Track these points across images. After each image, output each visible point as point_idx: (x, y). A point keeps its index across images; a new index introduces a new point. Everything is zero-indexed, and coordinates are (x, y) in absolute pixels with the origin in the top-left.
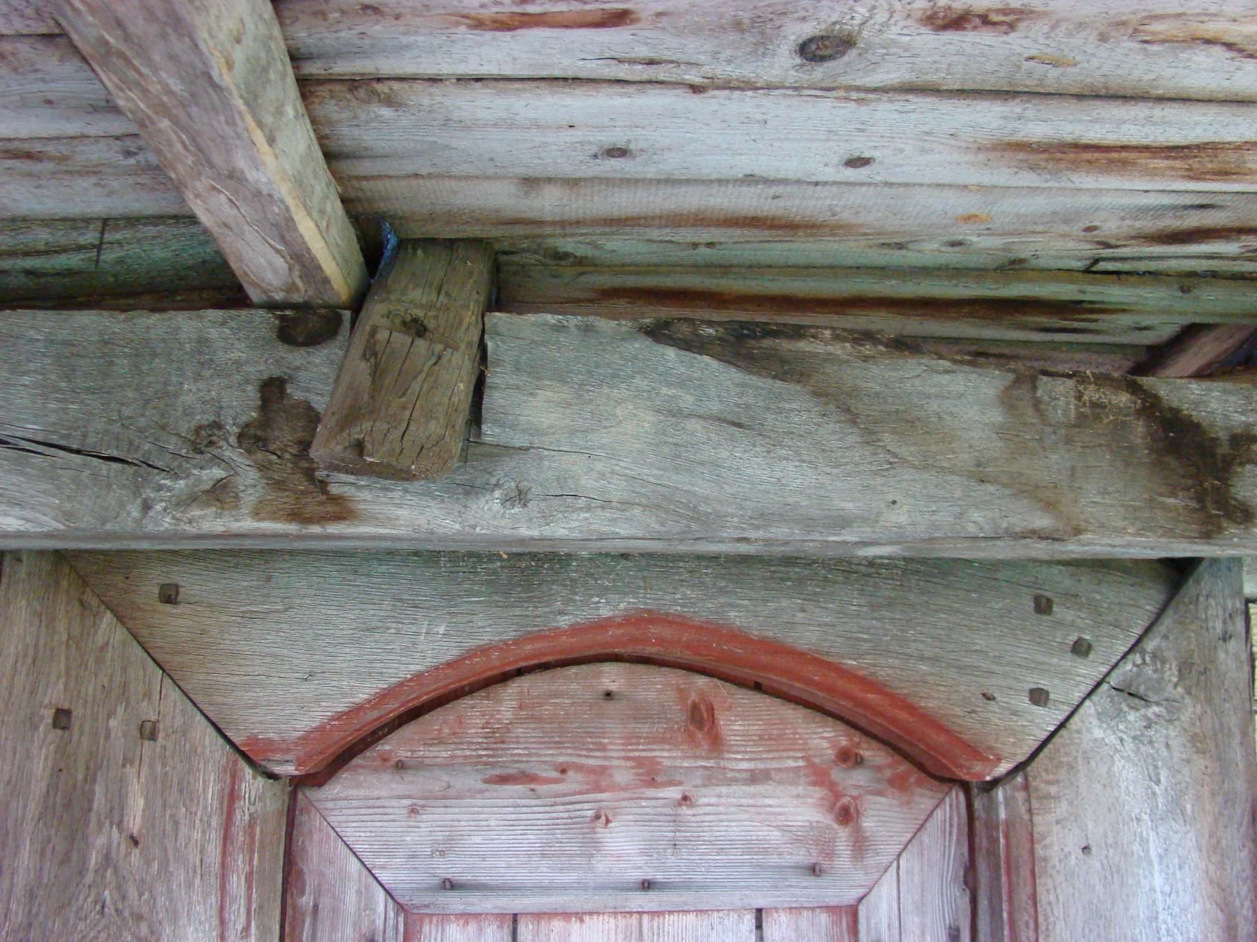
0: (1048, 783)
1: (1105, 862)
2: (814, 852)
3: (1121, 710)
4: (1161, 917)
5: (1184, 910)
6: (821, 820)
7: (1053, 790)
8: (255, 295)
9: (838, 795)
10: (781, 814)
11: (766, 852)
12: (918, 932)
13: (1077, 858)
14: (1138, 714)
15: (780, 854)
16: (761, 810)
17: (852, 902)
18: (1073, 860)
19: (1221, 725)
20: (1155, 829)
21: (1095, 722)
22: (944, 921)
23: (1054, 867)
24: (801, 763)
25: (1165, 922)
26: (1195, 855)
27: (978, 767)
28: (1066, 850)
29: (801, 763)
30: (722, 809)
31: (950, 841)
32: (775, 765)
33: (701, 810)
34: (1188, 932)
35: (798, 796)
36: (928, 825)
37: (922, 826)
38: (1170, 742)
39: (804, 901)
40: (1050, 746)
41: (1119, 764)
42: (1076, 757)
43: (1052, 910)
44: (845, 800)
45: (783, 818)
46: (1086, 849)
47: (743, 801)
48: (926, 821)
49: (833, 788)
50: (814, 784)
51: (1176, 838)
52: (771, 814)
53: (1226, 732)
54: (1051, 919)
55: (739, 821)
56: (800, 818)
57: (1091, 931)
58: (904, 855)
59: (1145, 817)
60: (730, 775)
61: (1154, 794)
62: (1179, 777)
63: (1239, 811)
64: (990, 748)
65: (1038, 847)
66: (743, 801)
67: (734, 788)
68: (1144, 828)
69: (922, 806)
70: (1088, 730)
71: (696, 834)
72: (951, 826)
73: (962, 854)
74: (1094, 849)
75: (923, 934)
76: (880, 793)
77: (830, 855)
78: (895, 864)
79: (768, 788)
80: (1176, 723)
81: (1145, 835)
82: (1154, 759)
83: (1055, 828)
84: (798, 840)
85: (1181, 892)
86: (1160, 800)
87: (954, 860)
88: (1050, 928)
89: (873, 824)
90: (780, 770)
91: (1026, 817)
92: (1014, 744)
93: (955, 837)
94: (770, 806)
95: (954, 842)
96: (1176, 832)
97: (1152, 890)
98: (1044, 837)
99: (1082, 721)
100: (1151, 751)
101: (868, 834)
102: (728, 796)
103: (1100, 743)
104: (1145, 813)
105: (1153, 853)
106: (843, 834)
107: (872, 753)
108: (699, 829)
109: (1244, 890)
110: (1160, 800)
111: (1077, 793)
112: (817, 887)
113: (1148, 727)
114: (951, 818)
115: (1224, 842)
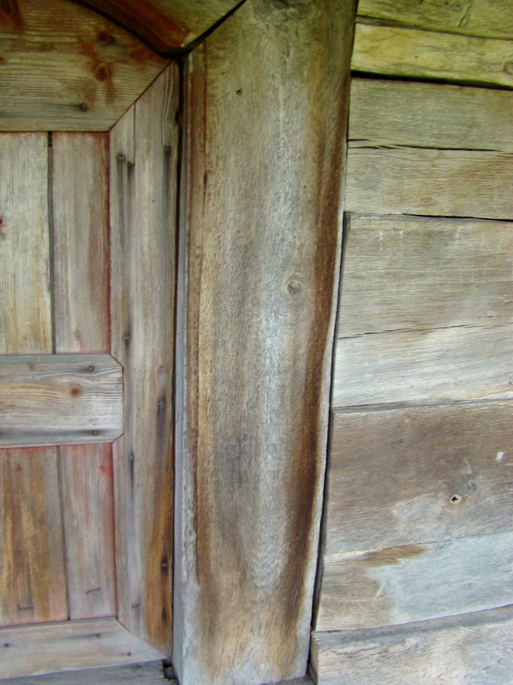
0: (219, 49)
1: (250, 100)
2: (82, 96)
3: (269, 8)
4: (281, 136)
5: (295, 133)
6: (87, 76)
7: (221, 53)
8: (109, 130)
9: (97, 62)
10: (61, 72)
11: (51, 95)
12: (146, 148)
13: (232, 97)
14: (280, 12)
15: (60, 97)
16: (49, 68)
17: (106, 129)
18: (230, 98)
19: (332, 25)
20: (283, 84)
21: (252, 13)
22: (162, 142)
23: (218, 101)
24: (74, 40)
25: (283, 139)
26: (306, 101)
27: (175, 36)
28: (227, 91)
29: (74, 40)
30: (23, 67)
31: (168, 95)
32: (57, 40)
33: (10, 67)
34: (296, 146)
35: (72, 61)
36: (154, 84)
37: (151, 84)
38: (299, 32)
39: (76, 128)
40: (222, 26)
41: (264, 41)
42: (237, 35)
43: (215, 126)
44: (102, 65)
45: (62, 74)
46: (239, 92)
47: (37, 62)
48: (154, 81)
49: (94, 55)
50: (82, 53)
51: (296, 90)
52: (52, 71)
53: (335, 29)
54: (214, 132)
55: (35, 75)
56: (74, 75)
57: (238, 141)
58: (139, 101)
59: (278, 76)
60: (28, 45)
61: (285, 62)
62: (302, 54)
63: (336, 79)
64: (182, 23)
65: (209, 88)
66: (37, 62)
67: (31, 54)
68: (276, 82)
69: (152, 72)
70: (247, 18)
71: (6, 82)
72: (169, 85)
73: (175, 103)
74: (244, 92)
75: (149, 149)
76: (124, 62)
77: (92, 98)
78: (133, 107)
79: (53, 54)
80: (304, 20)
81: (276, 86)
82: (287, 41)
83: (221, 77)
84: (70, 89)
85: (295, 123)
86: (288, 67)
87: (170, 107)
88: (213, 137)
89: (119, 81)
90: (60, 43)
91: (203, 70)
92: (198, 22)
93: (171, 93)
94: (54, 66)
95: (170, 95)
96: (296, 87)
97: (278, 119)
98: (213, 82)
99: (244, 13)
100: (287, 36)
101: (116, 87)
102: (27, 58)
103: (254, 27)
104: (278, 73)
105: (280, 97)
106: (101, 86)
107: (119, 36)
108: (9, 79)
109: (333, 125)
110: (288, 67)
111: (236, 57)
112: (84, 118)
113: (286, 20)
114: (169, 81)
115: (324, 96)
